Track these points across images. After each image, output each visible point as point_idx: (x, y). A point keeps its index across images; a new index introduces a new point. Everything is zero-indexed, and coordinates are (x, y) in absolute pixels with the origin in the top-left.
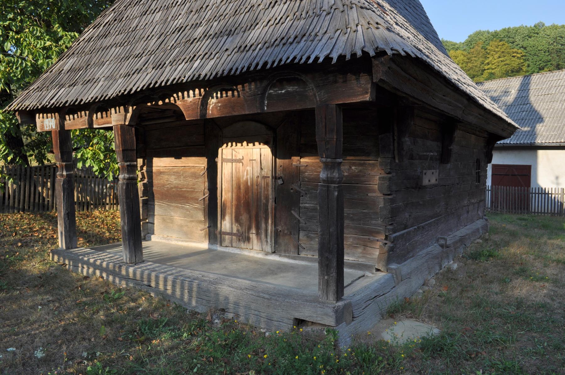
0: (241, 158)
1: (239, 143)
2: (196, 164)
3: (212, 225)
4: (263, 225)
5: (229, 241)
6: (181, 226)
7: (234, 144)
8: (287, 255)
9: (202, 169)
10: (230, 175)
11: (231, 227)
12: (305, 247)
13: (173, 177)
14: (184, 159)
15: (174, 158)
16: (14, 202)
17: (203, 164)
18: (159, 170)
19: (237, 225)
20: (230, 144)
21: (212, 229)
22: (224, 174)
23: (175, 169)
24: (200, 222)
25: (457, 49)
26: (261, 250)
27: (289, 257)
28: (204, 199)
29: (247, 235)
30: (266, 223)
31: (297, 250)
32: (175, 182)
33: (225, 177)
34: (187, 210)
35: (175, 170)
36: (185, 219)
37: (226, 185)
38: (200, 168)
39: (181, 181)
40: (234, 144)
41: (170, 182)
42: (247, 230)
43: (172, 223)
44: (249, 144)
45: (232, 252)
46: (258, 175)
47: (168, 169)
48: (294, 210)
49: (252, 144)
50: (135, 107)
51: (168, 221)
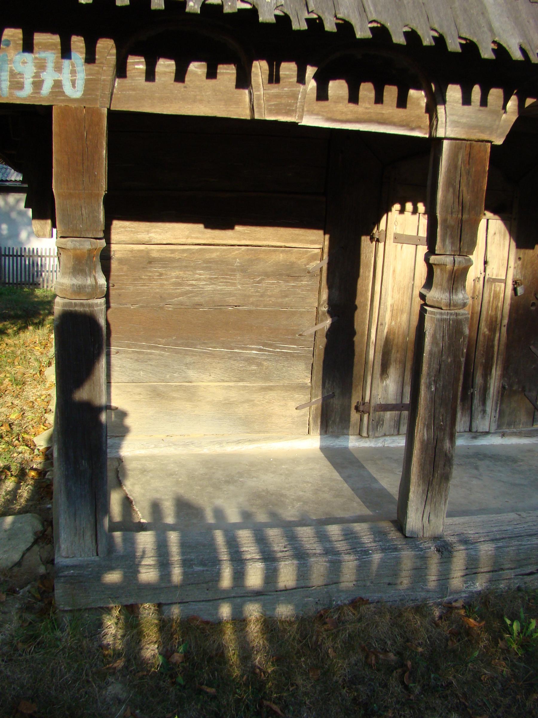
2: (294, 241)
3: (337, 391)
4: (479, 380)
5: (392, 423)
6: (228, 404)
9: (316, 254)
10: (409, 274)
13: (202, 274)
14: (238, 228)
15: (201, 226)
16: (29, 278)
18: (148, 252)
20: (409, 206)
21: (336, 402)
23: (211, 251)
24: (301, 387)
26: (467, 429)
27: (520, 434)
30: (487, 374)
31: (531, 420)
32: (209, 288)
34: (250, 360)
35: (214, 255)
36: (241, 384)
37: (396, 296)
38: (307, 252)
39: (233, 284)
41: (188, 288)
43: (189, 400)
45: (392, 445)
47: (184, 251)
50: (529, 101)
51: (175, 395)
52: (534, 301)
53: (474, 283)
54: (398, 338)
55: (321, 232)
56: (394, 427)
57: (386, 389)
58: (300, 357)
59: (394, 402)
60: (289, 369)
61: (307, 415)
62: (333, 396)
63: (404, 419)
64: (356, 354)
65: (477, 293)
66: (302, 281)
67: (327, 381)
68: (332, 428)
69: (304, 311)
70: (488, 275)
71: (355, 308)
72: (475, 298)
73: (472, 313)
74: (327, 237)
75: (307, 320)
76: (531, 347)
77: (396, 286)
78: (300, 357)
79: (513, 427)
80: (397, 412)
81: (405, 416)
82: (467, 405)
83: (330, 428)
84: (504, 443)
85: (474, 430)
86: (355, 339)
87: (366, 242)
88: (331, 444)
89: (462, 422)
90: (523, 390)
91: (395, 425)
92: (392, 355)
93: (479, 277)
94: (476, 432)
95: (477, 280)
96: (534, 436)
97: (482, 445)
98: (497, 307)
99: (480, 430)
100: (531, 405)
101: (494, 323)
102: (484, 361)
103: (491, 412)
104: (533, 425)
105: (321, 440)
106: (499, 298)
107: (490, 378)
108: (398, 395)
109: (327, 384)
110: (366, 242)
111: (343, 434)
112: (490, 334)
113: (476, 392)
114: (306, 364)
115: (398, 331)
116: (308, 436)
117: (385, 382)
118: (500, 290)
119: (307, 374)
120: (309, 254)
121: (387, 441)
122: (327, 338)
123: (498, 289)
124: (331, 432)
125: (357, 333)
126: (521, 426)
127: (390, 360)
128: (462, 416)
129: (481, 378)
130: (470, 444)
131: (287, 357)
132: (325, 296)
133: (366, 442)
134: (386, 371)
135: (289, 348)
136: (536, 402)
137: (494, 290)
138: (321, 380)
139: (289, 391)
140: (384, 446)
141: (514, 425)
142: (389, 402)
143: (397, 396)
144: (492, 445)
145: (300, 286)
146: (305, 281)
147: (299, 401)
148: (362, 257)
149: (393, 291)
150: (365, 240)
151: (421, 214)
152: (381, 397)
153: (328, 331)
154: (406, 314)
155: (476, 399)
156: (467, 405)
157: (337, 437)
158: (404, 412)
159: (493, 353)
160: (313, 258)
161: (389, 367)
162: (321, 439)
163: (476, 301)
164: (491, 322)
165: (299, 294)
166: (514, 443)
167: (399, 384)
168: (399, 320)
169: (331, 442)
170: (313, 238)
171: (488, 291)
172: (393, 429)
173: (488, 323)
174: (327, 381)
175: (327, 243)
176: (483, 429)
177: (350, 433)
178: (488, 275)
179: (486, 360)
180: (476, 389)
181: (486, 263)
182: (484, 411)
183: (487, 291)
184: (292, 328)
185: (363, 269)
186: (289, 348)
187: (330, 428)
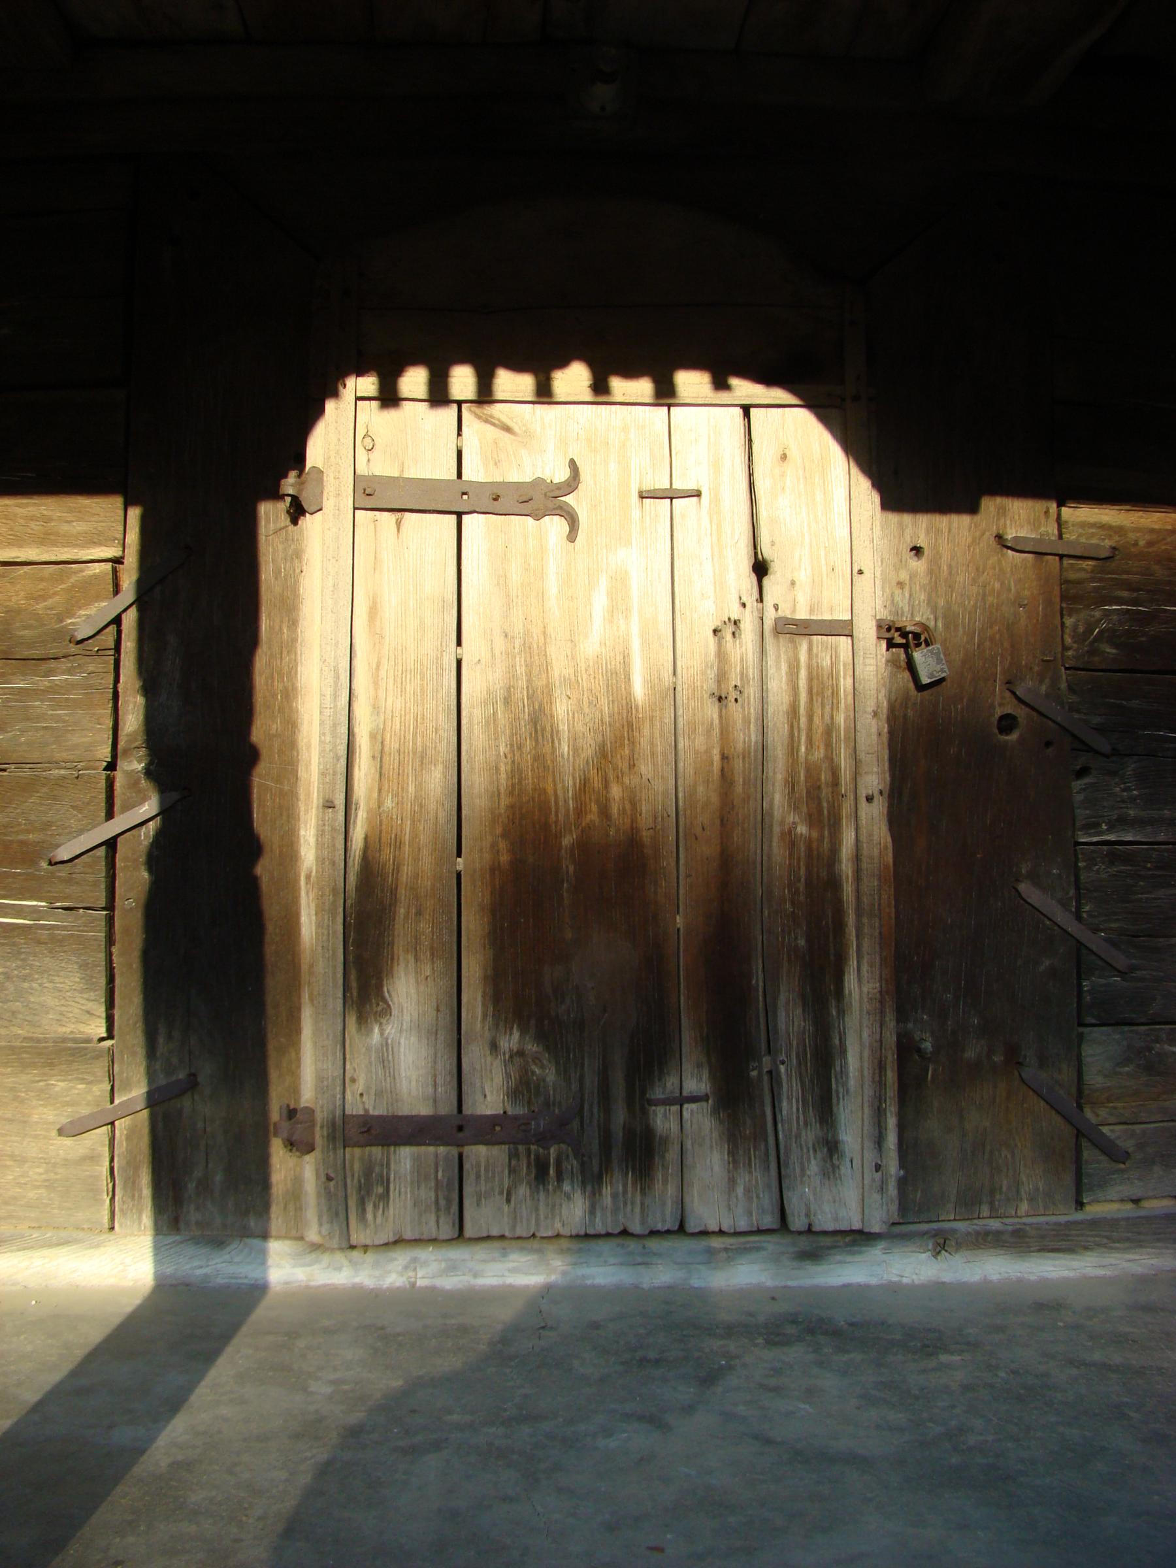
0: (561, 475)
1: (517, 366)
3: (207, 1070)
7: (462, 380)
8: (995, 1224)
11: (446, 1064)
12: (1129, 1145)
17: (92, 541)
19: (511, 1040)
20: (414, 381)
22: (374, 611)
25: (323, 831)
26: (769, 1221)
28: (111, 844)
29: (620, 1116)
31: (1069, 1178)
33: (377, 636)
40: (462, 380)
42: (618, 1079)
44: (618, 385)
45: (449, 1283)
46: (735, 612)
48: (1034, 878)
49: (643, 387)
52: (1008, 710)
53: (720, 645)
54: (416, 860)
55: (118, 501)
56: (438, 1209)
57: (385, 1058)
58: (61, 941)
59: (425, 1110)
60: (26, 985)
61: (100, 1156)
62: (192, 1084)
63: (478, 1177)
64: (270, 927)
65: (734, 679)
66: (48, 674)
67: (162, 1030)
68: (197, 1209)
69: (64, 777)
70: (776, 607)
71: (252, 756)
72: (731, 698)
73: (724, 758)
74: (135, 513)
75: (73, 807)
76: (1023, 887)
77: (384, 661)
78: (61, 941)
79: (985, 1211)
80: (441, 1149)
81: (478, 1165)
82: (749, 1122)
83: (192, 1207)
84: (947, 1277)
85: (797, 1222)
86: (262, 869)
87: (275, 522)
88: (199, 1272)
89: (740, 1190)
90: (1014, 1058)
91: (442, 1202)
92: (104, 894)
93: (734, 616)
94: (810, 1231)
95: (730, 629)
96: (1086, 1248)
97: (845, 1286)
98: (830, 730)
99: (825, 1220)
100: (1058, 1120)
101: (826, 792)
102: (802, 942)
103: (863, 1149)
104: (1080, 1205)
105: (156, 1255)
106: (835, 693)
107: (842, 1012)
108: (440, 1081)
109: (161, 1040)
110: (275, 522)
111: (245, 1233)
112: (815, 835)
113: (782, 1068)
114: (84, 966)
115: (414, 836)
116: (111, 1236)
117: (376, 1030)
118: (834, 663)
119: (90, 1006)
120: (73, 579)
121: (425, 1264)
122: (150, 870)
123: (826, 662)
124: (198, 1223)
125: (267, 849)
126: (1024, 1207)
127: (391, 944)
128: (736, 1167)
129: (799, 1011)
130: (790, 1283)
131: (14, 944)
132: (133, 720)
133: (339, 1269)
134: (379, 987)
135: (19, 912)
136: (1080, 1107)
137: (809, 667)
138: (140, 1026)
139: (33, 1065)
140: (413, 1285)
141: (991, 1203)
142: (405, 1110)
143: (435, 1085)
144: (893, 1289)
145: (46, 691)
146: (63, 673)
147: (68, 1104)
148: (263, 577)
149: (376, 684)
150: (271, 514)
151: (464, 406)
152: (368, 1088)
153: (152, 844)
154: (440, 767)
155: (790, 1099)
156: (749, 1122)
157: (218, 1243)
158: (474, 1148)
159: (839, 912)
160: (85, 593)
161: (390, 973)
162: (158, 1249)
163: (735, 711)
164: (814, 790)
165: (40, 718)
166: (995, 1277)
167: (441, 1038)
168: (411, 789)
169: (196, 1263)
170: (828, 777)
171: (784, 667)
172: (433, 1217)
173: (802, 789)
174: (162, 1030)
175: (133, 537)
176: (836, 1219)
177: (274, 1232)
178: (776, 607)
179: (807, 941)
180: (783, 1057)
181: (760, 569)
182: (831, 1147)
183: (778, 668)
184: (21, 837)
185: (269, 615)
186: (19, 912)
187: (192, 1207)
